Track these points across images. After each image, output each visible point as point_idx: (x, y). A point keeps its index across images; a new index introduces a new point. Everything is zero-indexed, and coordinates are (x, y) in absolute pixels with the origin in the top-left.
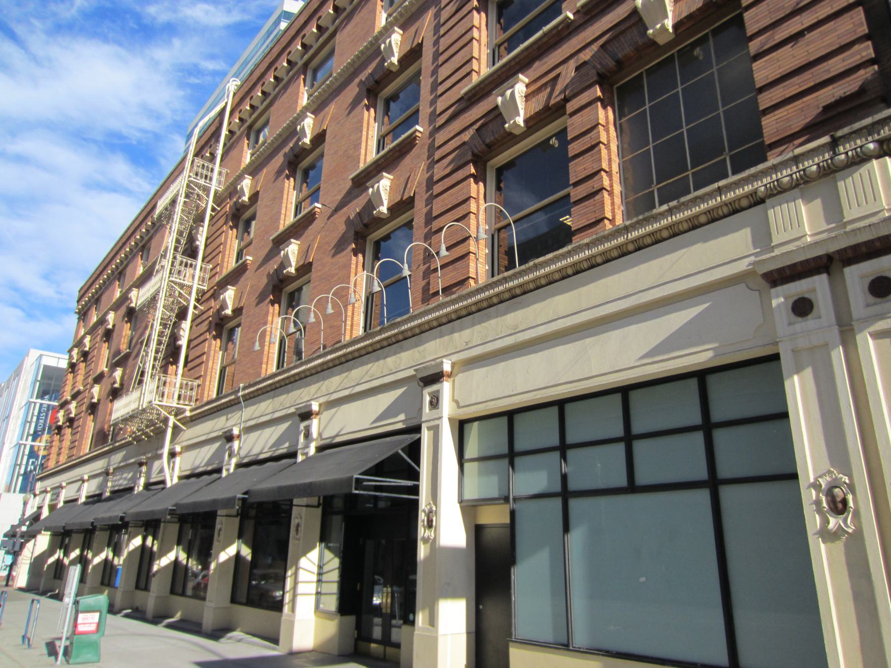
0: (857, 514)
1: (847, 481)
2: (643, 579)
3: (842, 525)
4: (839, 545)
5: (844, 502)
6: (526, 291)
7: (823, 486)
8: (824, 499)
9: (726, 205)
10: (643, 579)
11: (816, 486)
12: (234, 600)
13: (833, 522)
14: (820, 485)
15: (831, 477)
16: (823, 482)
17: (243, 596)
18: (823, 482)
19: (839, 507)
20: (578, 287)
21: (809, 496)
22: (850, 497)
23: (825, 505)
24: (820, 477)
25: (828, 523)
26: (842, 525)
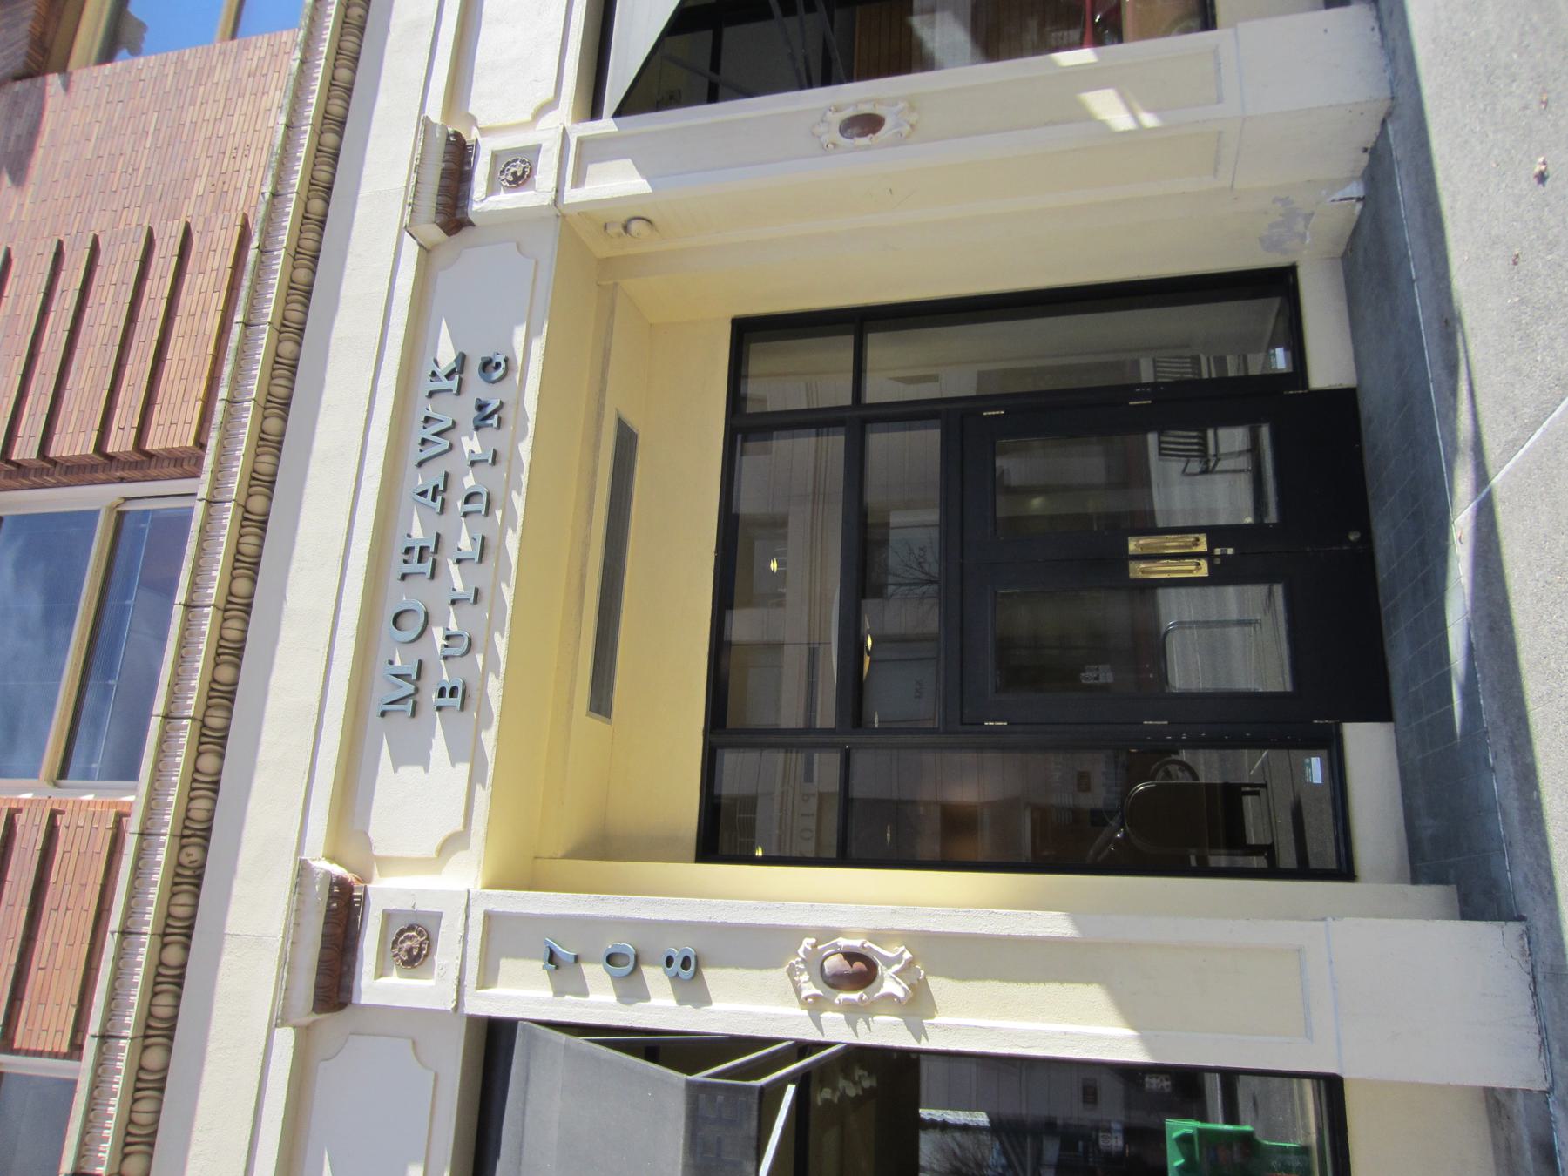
0: (878, 936)
1: (813, 940)
2: (774, 566)
3: (896, 967)
4: (939, 986)
5: (851, 956)
6: (286, 367)
7: (818, 992)
8: (843, 996)
9: (165, 935)
10: (774, 566)
11: (815, 1006)
12: (749, 333)
13: (890, 984)
14: (815, 997)
15: (801, 971)
16: (810, 989)
17: (784, 382)
18: (810, 989)
19: (860, 971)
20: (309, 451)
21: (837, 1030)
22: (843, 942)
23: (855, 996)
24: (798, 991)
25: (891, 996)
26: (896, 967)
